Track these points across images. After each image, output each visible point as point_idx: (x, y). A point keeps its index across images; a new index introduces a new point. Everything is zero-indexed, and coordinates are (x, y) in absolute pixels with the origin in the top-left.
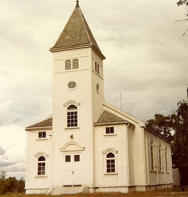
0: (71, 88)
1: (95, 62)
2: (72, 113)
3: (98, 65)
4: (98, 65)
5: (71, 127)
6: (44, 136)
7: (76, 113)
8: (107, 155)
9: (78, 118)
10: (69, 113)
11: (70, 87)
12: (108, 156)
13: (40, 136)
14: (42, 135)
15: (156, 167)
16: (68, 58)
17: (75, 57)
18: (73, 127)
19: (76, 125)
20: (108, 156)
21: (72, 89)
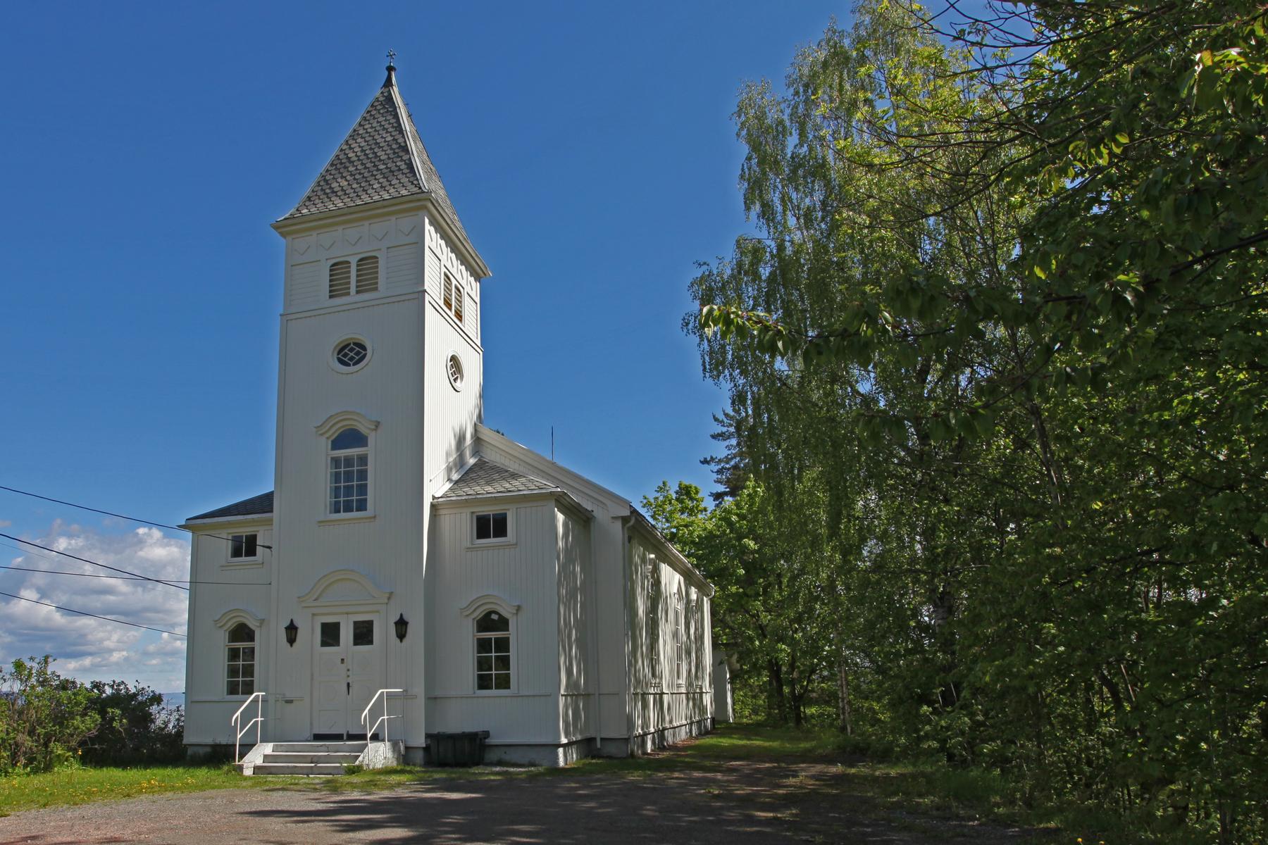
0: (349, 365)
1: (446, 275)
2: (348, 461)
3: (457, 288)
4: (457, 288)
5: (342, 515)
6: (251, 551)
7: (363, 460)
8: (333, 442)
9: (369, 464)
10: (336, 462)
11: (347, 364)
12: (337, 444)
13: (237, 553)
14: (246, 547)
15: (644, 577)
16: (338, 254)
17: (365, 250)
18: (450, 376)
19: (362, 506)
20: (337, 444)
21: (352, 369)
